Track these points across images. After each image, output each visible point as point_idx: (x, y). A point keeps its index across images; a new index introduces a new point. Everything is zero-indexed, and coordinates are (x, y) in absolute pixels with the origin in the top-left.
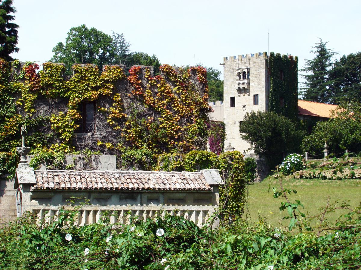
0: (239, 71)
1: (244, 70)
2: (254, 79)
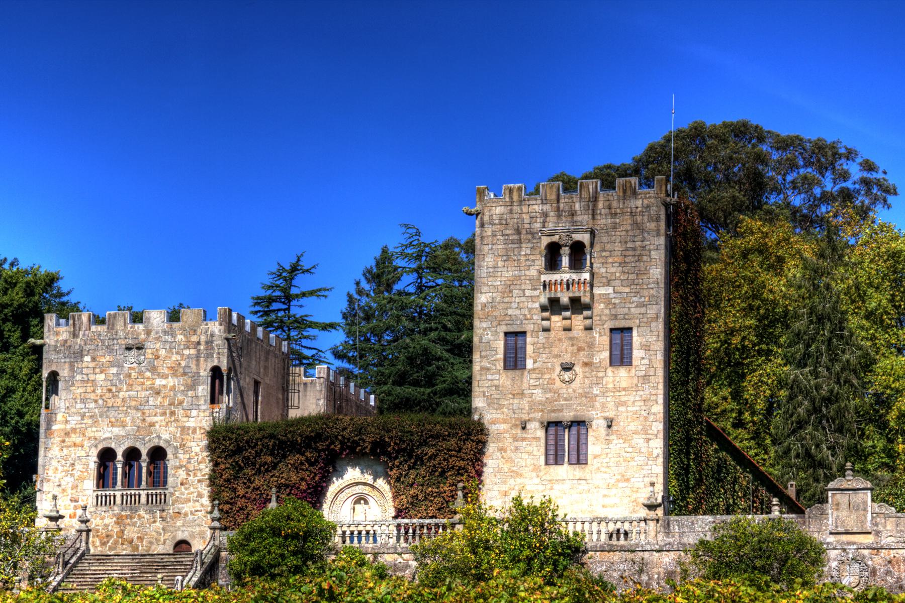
0: (556, 238)
1: (577, 237)
2: (613, 270)
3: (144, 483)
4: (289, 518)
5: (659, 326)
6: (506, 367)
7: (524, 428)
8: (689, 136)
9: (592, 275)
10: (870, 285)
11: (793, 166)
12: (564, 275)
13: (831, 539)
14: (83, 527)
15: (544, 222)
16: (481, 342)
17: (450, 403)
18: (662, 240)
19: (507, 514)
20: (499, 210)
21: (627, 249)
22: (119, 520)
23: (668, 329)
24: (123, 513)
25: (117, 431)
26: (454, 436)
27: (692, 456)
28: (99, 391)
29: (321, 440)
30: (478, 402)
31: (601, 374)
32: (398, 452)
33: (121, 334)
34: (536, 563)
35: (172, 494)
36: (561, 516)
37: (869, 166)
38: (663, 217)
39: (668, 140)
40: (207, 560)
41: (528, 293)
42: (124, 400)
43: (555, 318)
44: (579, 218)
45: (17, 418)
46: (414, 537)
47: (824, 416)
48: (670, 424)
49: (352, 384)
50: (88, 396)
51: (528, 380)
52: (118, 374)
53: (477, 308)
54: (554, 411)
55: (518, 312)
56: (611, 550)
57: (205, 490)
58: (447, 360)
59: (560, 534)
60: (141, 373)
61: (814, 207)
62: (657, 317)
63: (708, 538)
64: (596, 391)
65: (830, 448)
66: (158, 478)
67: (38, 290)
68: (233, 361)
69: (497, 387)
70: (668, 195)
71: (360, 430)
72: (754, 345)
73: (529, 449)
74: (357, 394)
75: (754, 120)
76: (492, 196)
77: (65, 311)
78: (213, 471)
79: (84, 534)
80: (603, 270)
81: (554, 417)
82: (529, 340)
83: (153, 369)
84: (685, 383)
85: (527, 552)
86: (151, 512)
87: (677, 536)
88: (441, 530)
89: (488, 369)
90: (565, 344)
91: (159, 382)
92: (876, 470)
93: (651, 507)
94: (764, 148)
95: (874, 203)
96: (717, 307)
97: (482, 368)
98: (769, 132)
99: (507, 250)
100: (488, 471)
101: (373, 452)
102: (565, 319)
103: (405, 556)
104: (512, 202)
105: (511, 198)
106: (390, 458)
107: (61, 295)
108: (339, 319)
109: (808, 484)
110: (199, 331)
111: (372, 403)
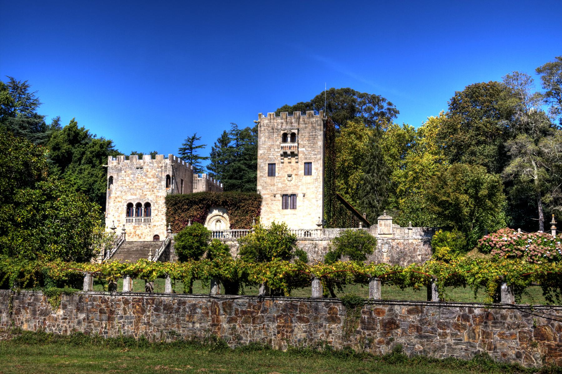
0: (286, 131)
1: (293, 131)
2: (305, 142)
3: (143, 215)
4: (195, 229)
5: (321, 162)
6: (269, 176)
7: (275, 197)
8: (330, 93)
9: (298, 144)
10: (391, 145)
11: (365, 104)
12: (289, 144)
13: (379, 236)
14: (123, 232)
15: (282, 126)
16: (260, 167)
17: (248, 186)
18: (322, 133)
19: (270, 228)
20: (266, 121)
21: (310, 135)
22: (134, 228)
23: (324, 163)
24: (136, 225)
25: (134, 197)
26: (251, 199)
27: (332, 206)
28: (127, 183)
29: (205, 200)
30: (259, 188)
31: (301, 178)
32: (231, 205)
33: (135, 163)
34: (280, 245)
35: (153, 219)
36: (288, 229)
37: (390, 104)
38: (322, 124)
39: (323, 94)
40: (167, 244)
41: (276, 150)
42: (136, 186)
43: (286, 159)
44: (294, 125)
45: (97, 191)
46: (238, 236)
47: (375, 190)
48: (324, 196)
49: (215, 180)
50: (123, 185)
51: (276, 180)
52: (134, 177)
53: (259, 155)
54: (285, 191)
55: (273, 157)
56: (305, 240)
57: (164, 218)
58: (247, 170)
59: (288, 234)
60: (142, 177)
61: (372, 118)
62: (320, 159)
63: (338, 237)
64: (299, 184)
65: (378, 201)
66: (148, 213)
67: (105, 146)
68: (174, 173)
69: (266, 182)
70: (324, 117)
71: (218, 197)
72: (353, 165)
73: (277, 204)
74: (216, 183)
75: (352, 88)
76: (264, 116)
77: (116, 154)
78: (167, 211)
79: (124, 234)
80: (302, 142)
81: (285, 193)
82: (277, 166)
83: (146, 175)
84: (330, 181)
85: (277, 241)
86: (145, 225)
87: (327, 235)
88: (247, 233)
89: (262, 176)
90: (289, 168)
91: (148, 180)
92: (392, 208)
93: (319, 225)
94: (355, 97)
95: (392, 116)
96: (340, 152)
97: (260, 176)
98: (357, 92)
99: (269, 135)
100: (262, 211)
101: (223, 204)
102: (289, 159)
103: (235, 242)
104: (271, 119)
105: (270, 117)
106: (229, 207)
107: (112, 147)
108: (209, 156)
109: (370, 214)
110: (162, 162)
111: (222, 186)
